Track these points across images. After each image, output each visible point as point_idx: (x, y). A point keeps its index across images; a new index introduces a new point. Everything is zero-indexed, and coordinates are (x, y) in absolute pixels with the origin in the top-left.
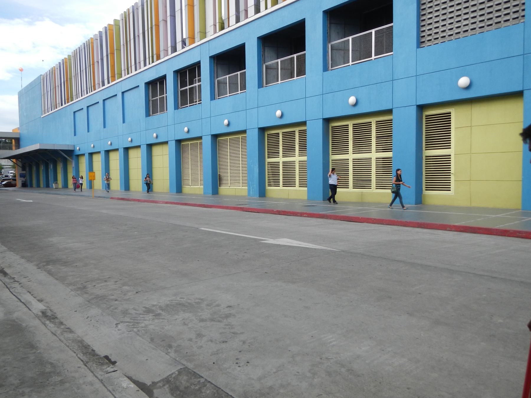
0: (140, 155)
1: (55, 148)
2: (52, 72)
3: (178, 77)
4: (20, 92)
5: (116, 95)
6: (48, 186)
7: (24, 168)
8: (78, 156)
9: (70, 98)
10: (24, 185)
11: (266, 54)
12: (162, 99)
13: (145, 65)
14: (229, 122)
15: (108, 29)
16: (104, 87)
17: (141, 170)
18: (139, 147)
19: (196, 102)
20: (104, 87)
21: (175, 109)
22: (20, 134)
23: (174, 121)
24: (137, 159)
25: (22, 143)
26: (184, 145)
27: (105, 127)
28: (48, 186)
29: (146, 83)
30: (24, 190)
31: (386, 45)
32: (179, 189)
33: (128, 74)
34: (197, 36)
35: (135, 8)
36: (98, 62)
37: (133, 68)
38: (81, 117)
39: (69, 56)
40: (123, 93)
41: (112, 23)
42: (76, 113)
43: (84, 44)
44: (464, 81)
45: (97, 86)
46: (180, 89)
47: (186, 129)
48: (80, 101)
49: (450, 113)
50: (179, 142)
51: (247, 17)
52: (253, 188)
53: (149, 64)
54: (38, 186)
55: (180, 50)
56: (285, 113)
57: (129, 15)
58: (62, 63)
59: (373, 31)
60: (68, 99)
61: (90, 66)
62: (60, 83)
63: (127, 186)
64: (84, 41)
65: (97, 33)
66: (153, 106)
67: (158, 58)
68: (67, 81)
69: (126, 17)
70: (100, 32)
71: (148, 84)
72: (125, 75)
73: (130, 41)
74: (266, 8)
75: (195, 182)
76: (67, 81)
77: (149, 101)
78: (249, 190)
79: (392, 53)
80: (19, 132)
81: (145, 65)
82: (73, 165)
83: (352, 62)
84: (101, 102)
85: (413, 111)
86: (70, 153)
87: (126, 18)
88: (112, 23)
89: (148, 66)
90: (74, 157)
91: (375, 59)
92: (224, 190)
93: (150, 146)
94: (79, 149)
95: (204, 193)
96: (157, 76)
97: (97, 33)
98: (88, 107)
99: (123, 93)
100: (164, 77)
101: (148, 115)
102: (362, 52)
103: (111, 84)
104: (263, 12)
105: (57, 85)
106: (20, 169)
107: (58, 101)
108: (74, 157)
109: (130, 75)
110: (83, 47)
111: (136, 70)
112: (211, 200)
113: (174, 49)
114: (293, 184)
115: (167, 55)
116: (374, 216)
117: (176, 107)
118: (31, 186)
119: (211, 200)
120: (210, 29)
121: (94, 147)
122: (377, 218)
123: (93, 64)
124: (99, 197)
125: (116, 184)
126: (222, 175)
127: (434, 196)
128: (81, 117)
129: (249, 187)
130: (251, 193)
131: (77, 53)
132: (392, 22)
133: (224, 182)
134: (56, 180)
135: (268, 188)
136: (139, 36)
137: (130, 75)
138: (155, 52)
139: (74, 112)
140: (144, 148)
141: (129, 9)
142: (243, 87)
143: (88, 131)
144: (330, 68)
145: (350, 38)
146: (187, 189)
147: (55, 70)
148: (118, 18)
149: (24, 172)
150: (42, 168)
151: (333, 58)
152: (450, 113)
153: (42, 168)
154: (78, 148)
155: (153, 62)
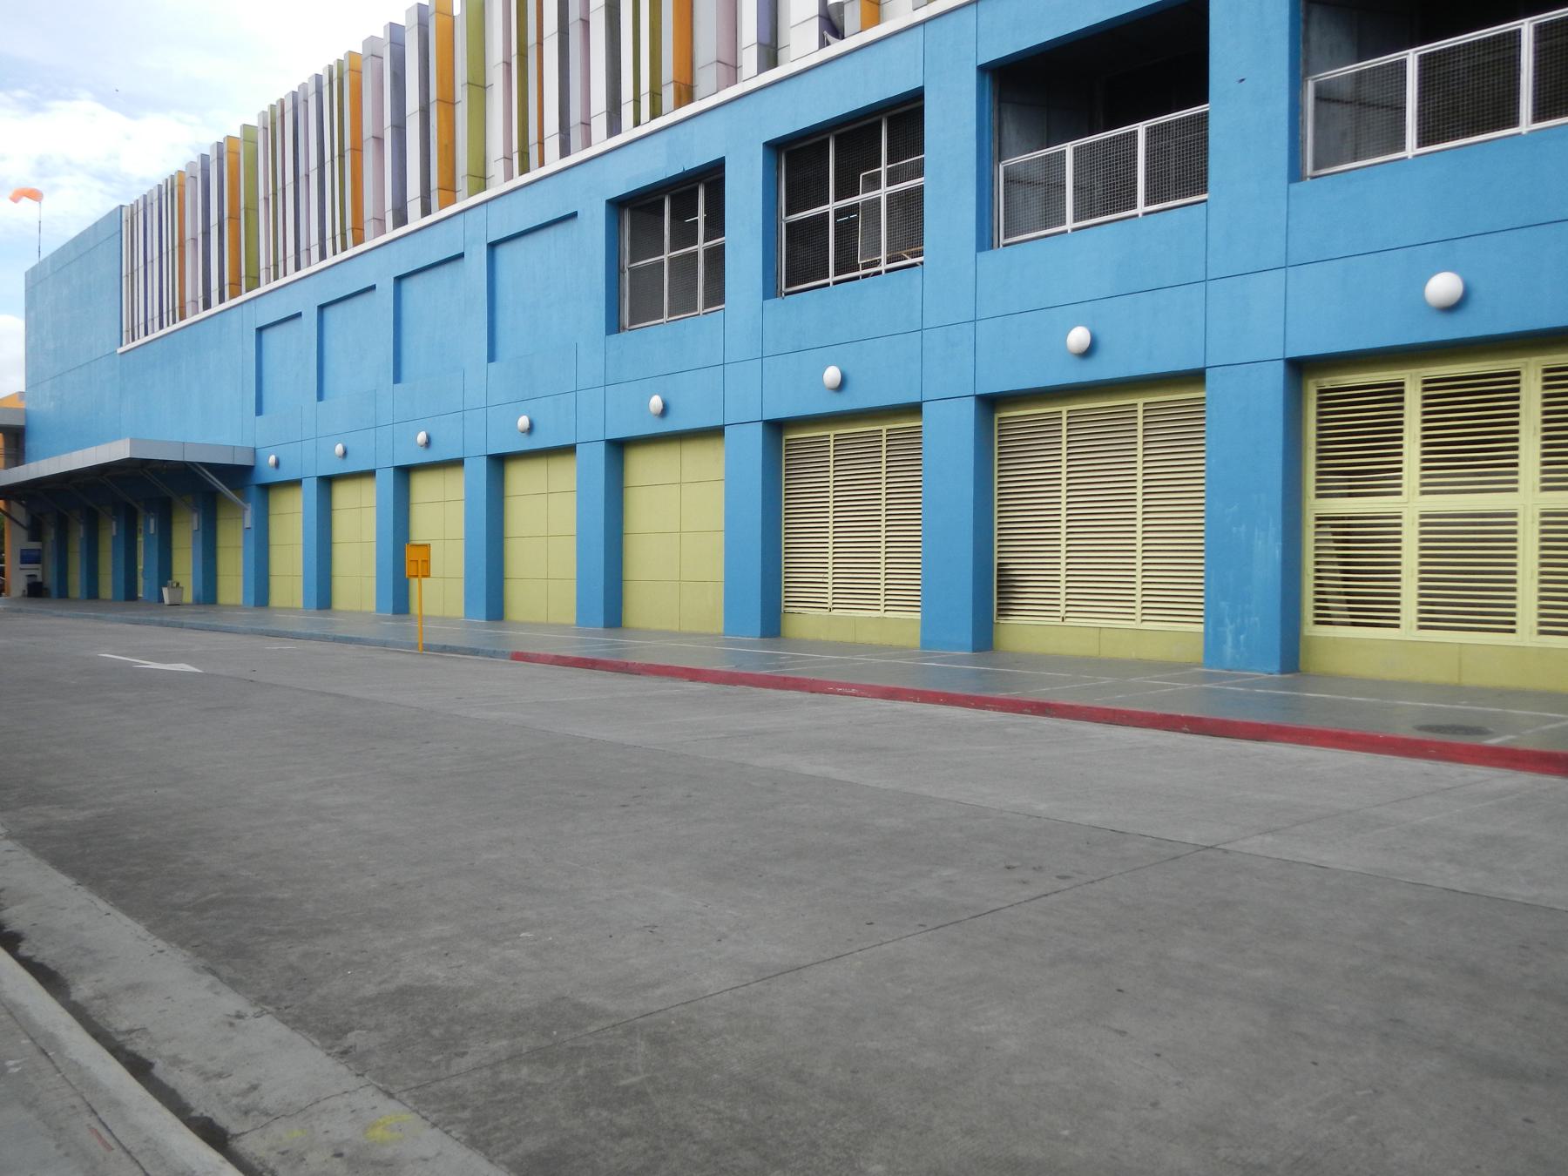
0: (460, 493)
1: (188, 458)
2: (173, 190)
3: (778, 168)
4: (33, 269)
5: (461, 256)
6: (130, 594)
7: (35, 532)
8: (267, 488)
9: (242, 277)
10: (36, 590)
11: (1314, 36)
12: (716, 258)
13: (323, 256)
14: (428, 437)
15: (346, 67)
16: (527, 178)
17: (572, 544)
18: (370, 474)
19: (877, 263)
20: (527, 178)
21: (765, 297)
22: (26, 414)
23: (755, 343)
24: (443, 512)
25: (31, 444)
26: (790, 443)
27: (397, 378)
28: (130, 594)
29: (610, 203)
30: (35, 605)
31: (1183, 171)
32: (772, 624)
33: (276, 278)
34: (462, 184)
35: (301, 98)
36: (379, 140)
37: (315, 251)
38: (291, 352)
39: (245, 127)
40: (492, 246)
41: (237, 133)
42: (266, 335)
43: (318, 78)
44: (1443, 286)
45: (369, 228)
46: (787, 219)
47: (656, 402)
48: (289, 288)
49: (1402, 384)
50: (776, 428)
51: (588, 143)
52: (1237, 633)
53: (335, 253)
54: (92, 593)
55: (415, 221)
56: (1104, 340)
57: (283, 116)
58: (326, 81)
59: (1141, 128)
60: (656, 95)
61: (342, 156)
62: (217, 221)
63: (323, 595)
64: (320, 69)
65: (380, 32)
66: (632, 300)
67: (254, 282)
68: (234, 217)
69: (274, 118)
70: (395, 31)
71: (617, 205)
72: (268, 282)
73: (540, 43)
74: (637, 123)
75: (854, 591)
76: (234, 217)
77: (620, 271)
78: (1213, 641)
79: (1204, 197)
80: (23, 405)
81: (323, 256)
82: (249, 520)
83: (1147, 204)
84: (477, 259)
85: (1275, 375)
86: (238, 476)
87: (273, 124)
88: (237, 133)
89: (330, 260)
90: (254, 493)
91: (1145, 214)
92: (1026, 630)
93: (405, 473)
94: (277, 464)
95: (925, 643)
96: (675, 170)
97: (194, 157)
98: (322, 308)
99: (492, 246)
100: (712, 176)
101: (614, 325)
102: (1108, 192)
103: (228, 304)
104: (629, 132)
105: (188, 235)
106: (23, 534)
107: (193, 289)
108: (254, 493)
109: (282, 281)
110: (156, 196)
111: (298, 268)
112: (753, 653)
113: (401, 218)
114: (1380, 612)
115: (384, 232)
116: (1405, 731)
117: (771, 290)
118: (63, 594)
119: (753, 653)
120: (496, 169)
121: (345, 453)
122: (1536, 748)
123: (357, 149)
124: (444, 649)
125: (444, 593)
126: (1017, 567)
127: (1342, 645)
128: (291, 352)
129: (1214, 623)
130: (1228, 649)
131: (282, 122)
132: (1205, 100)
133: (1030, 594)
134: (165, 573)
135: (1311, 630)
136: (586, 23)
137: (282, 281)
138: (668, 73)
139: (260, 330)
140: (386, 478)
141: (282, 102)
142: (716, 295)
143: (320, 397)
144: (1309, 170)
145: (1069, 148)
146: (811, 621)
147: (182, 186)
148: (254, 121)
149: (35, 545)
150: (110, 534)
151: (1012, 209)
152: (1402, 384)
153: (110, 534)
154: (272, 459)
155: (344, 249)
